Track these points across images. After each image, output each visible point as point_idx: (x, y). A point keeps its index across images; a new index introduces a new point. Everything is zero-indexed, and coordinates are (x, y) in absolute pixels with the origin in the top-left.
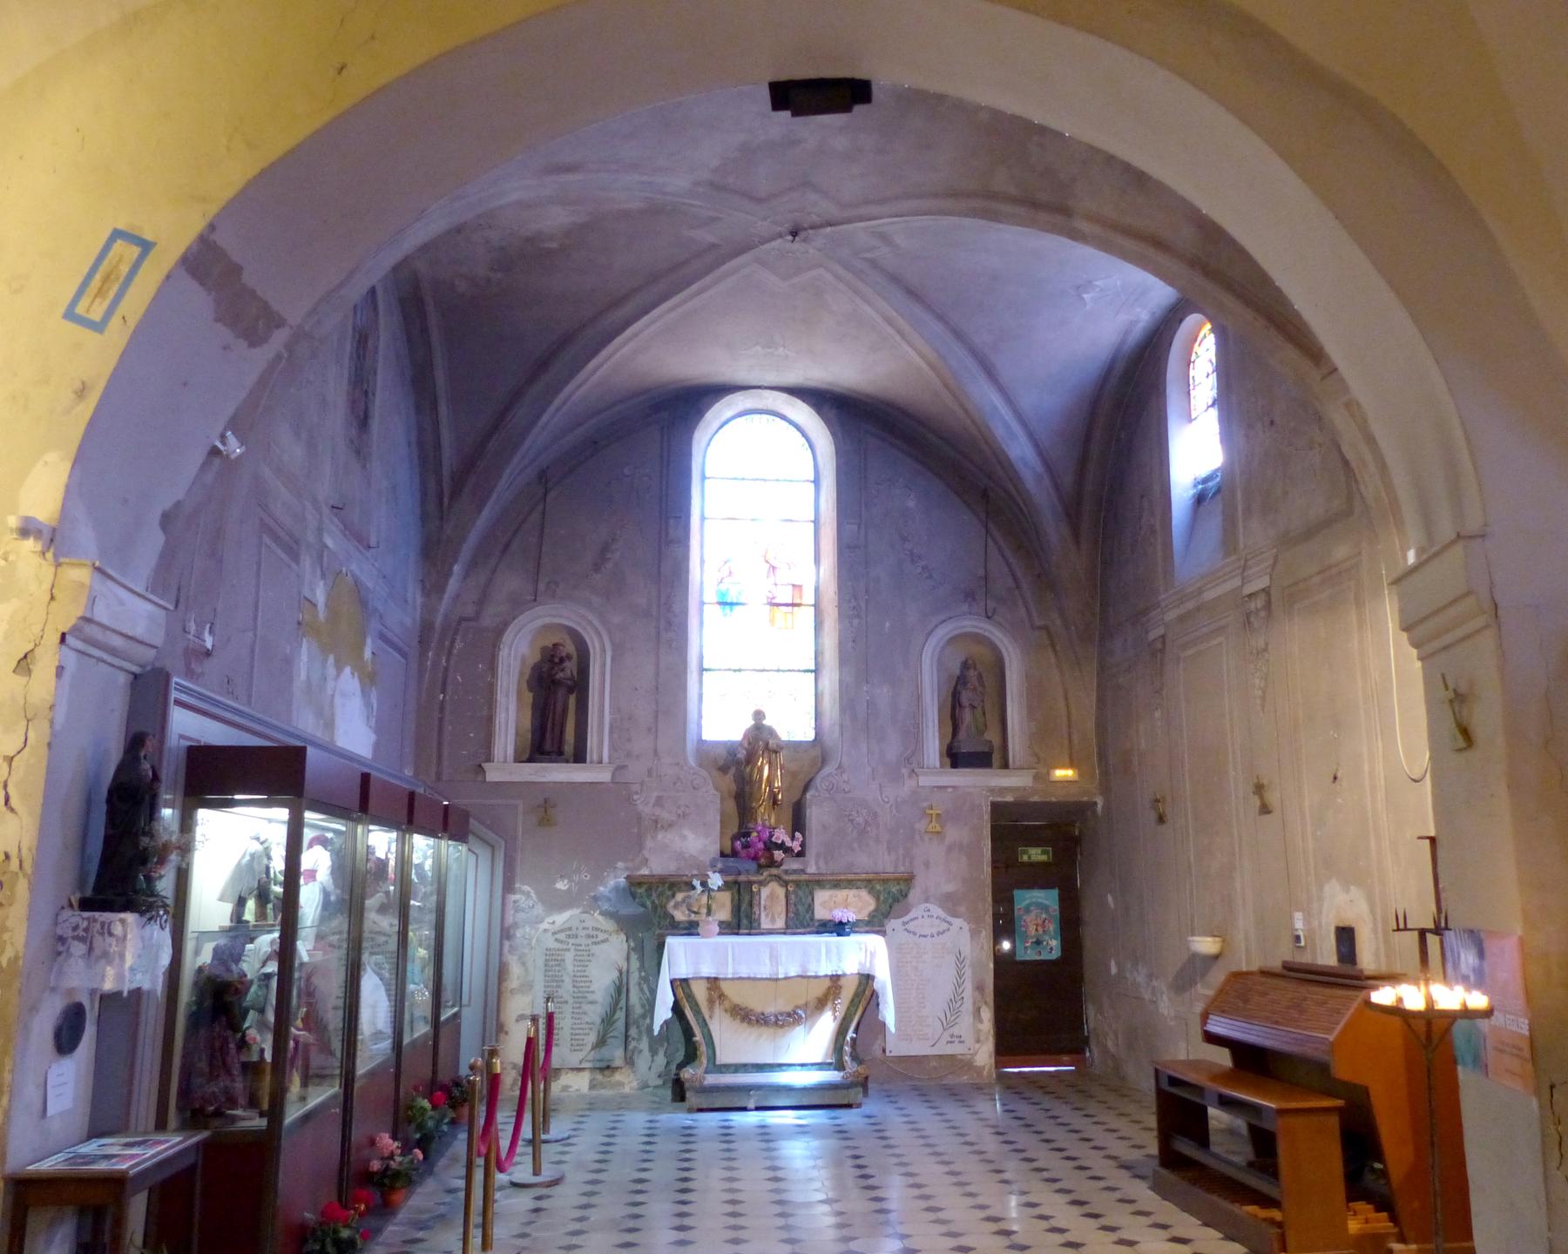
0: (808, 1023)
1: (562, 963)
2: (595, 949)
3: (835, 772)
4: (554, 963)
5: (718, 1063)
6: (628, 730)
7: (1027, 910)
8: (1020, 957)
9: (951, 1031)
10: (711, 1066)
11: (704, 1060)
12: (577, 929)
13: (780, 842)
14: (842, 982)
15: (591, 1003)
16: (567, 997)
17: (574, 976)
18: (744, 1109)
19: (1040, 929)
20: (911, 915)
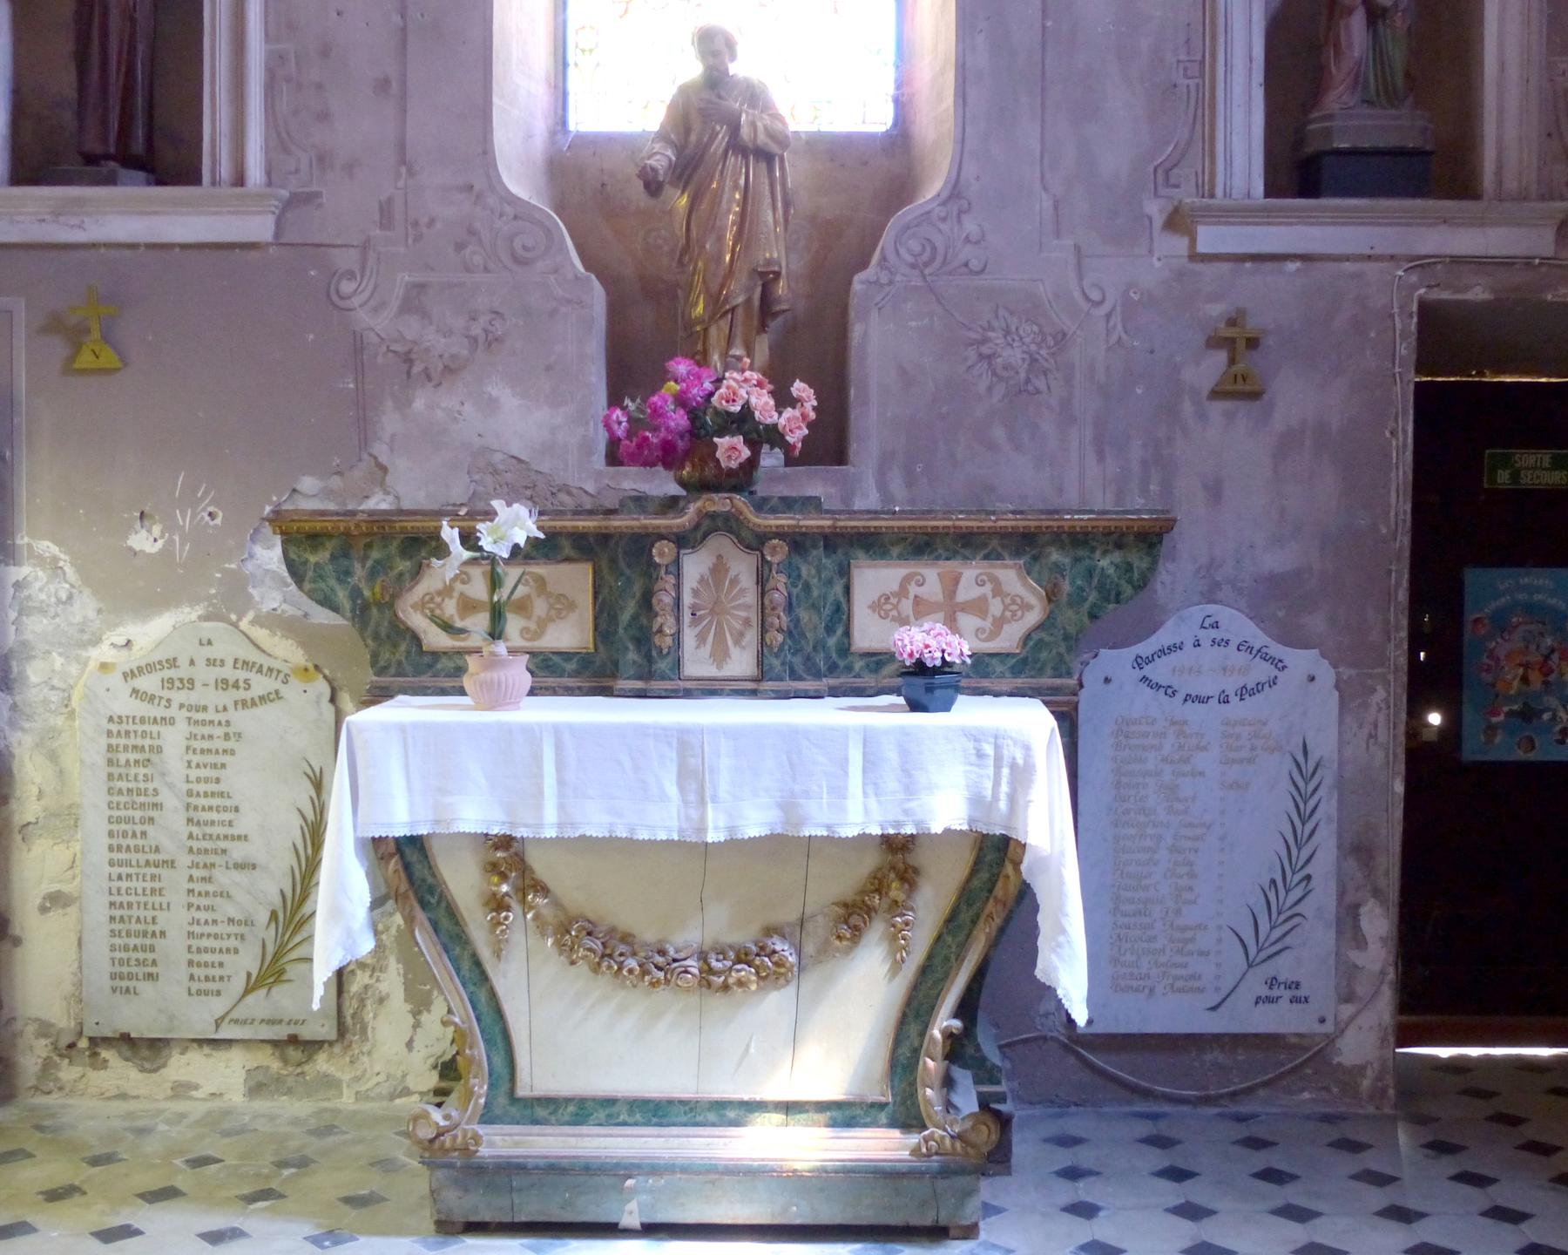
0: (810, 981)
1: (154, 758)
2: (242, 720)
3: (940, 211)
4: (132, 756)
5: (522, 1091)
6: (319, 86)
7: (1501, 624)
8: (1474, 749)
9: (1268, 969)
10: (502, 1100)
11: (481, 1088)
12: (192, 663)
13: (736, 408)
14: (920, 858)
15: (240, 866)
16: (170, 849)
17: (190, 793)
18: (609, 1230)
19: (1536, 678)
20: (1162, 638)
